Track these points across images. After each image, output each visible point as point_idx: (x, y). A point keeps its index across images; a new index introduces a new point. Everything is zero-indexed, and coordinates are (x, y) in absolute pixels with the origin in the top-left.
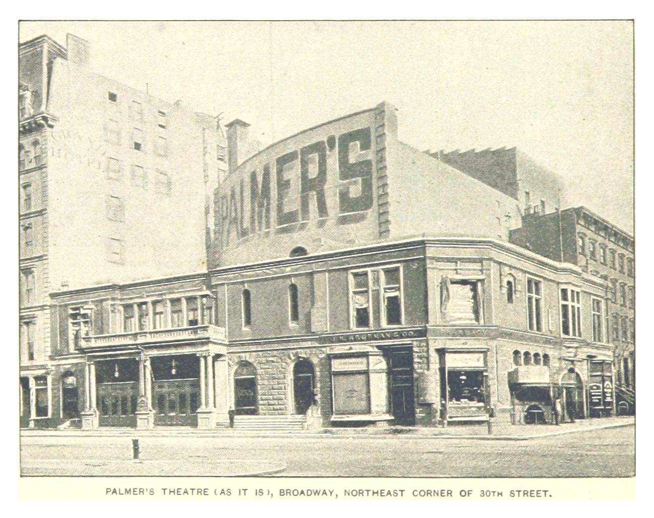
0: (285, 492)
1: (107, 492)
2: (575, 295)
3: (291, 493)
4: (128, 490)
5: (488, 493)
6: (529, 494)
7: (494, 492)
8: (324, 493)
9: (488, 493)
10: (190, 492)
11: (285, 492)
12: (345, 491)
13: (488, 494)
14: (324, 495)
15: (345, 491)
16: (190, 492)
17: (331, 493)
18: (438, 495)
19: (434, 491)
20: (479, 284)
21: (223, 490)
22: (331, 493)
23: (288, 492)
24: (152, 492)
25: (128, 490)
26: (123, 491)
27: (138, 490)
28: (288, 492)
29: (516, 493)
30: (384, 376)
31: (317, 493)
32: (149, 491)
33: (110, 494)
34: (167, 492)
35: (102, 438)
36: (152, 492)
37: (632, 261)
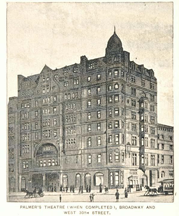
0: (122, 207)
1: (21, 207)
2: (134, 104)
3: (125, 208)
4: (30, 206)
5: (83, 212)
6: (101, 213)
7: (85, 212)
8: (139, 207)
9: (83, 212)
10: (56, 207)
11: (122, 207)
12: (82, 208)
13: (83, 213)
14: (139, 208)
15: (82, 208)
16: (56, 207)
17: (142, 207)
18: (151, 208)
19: (150, 207)
20: (172, 193)
21: (148, 206)
22: (142, 207)
23: (124, 207)
24: (40, 207)
25: (30, 206)
26: (28, 207)
27: (34, 207)
28: (124, 207)
29: (95, 213)
30: (116, 180)
31: (136, 207)
32: (39, 207)
33: (22, 208)
34: (47, 207)
35: (64, 196)
36: (40, 207)
37: (171, 138)
